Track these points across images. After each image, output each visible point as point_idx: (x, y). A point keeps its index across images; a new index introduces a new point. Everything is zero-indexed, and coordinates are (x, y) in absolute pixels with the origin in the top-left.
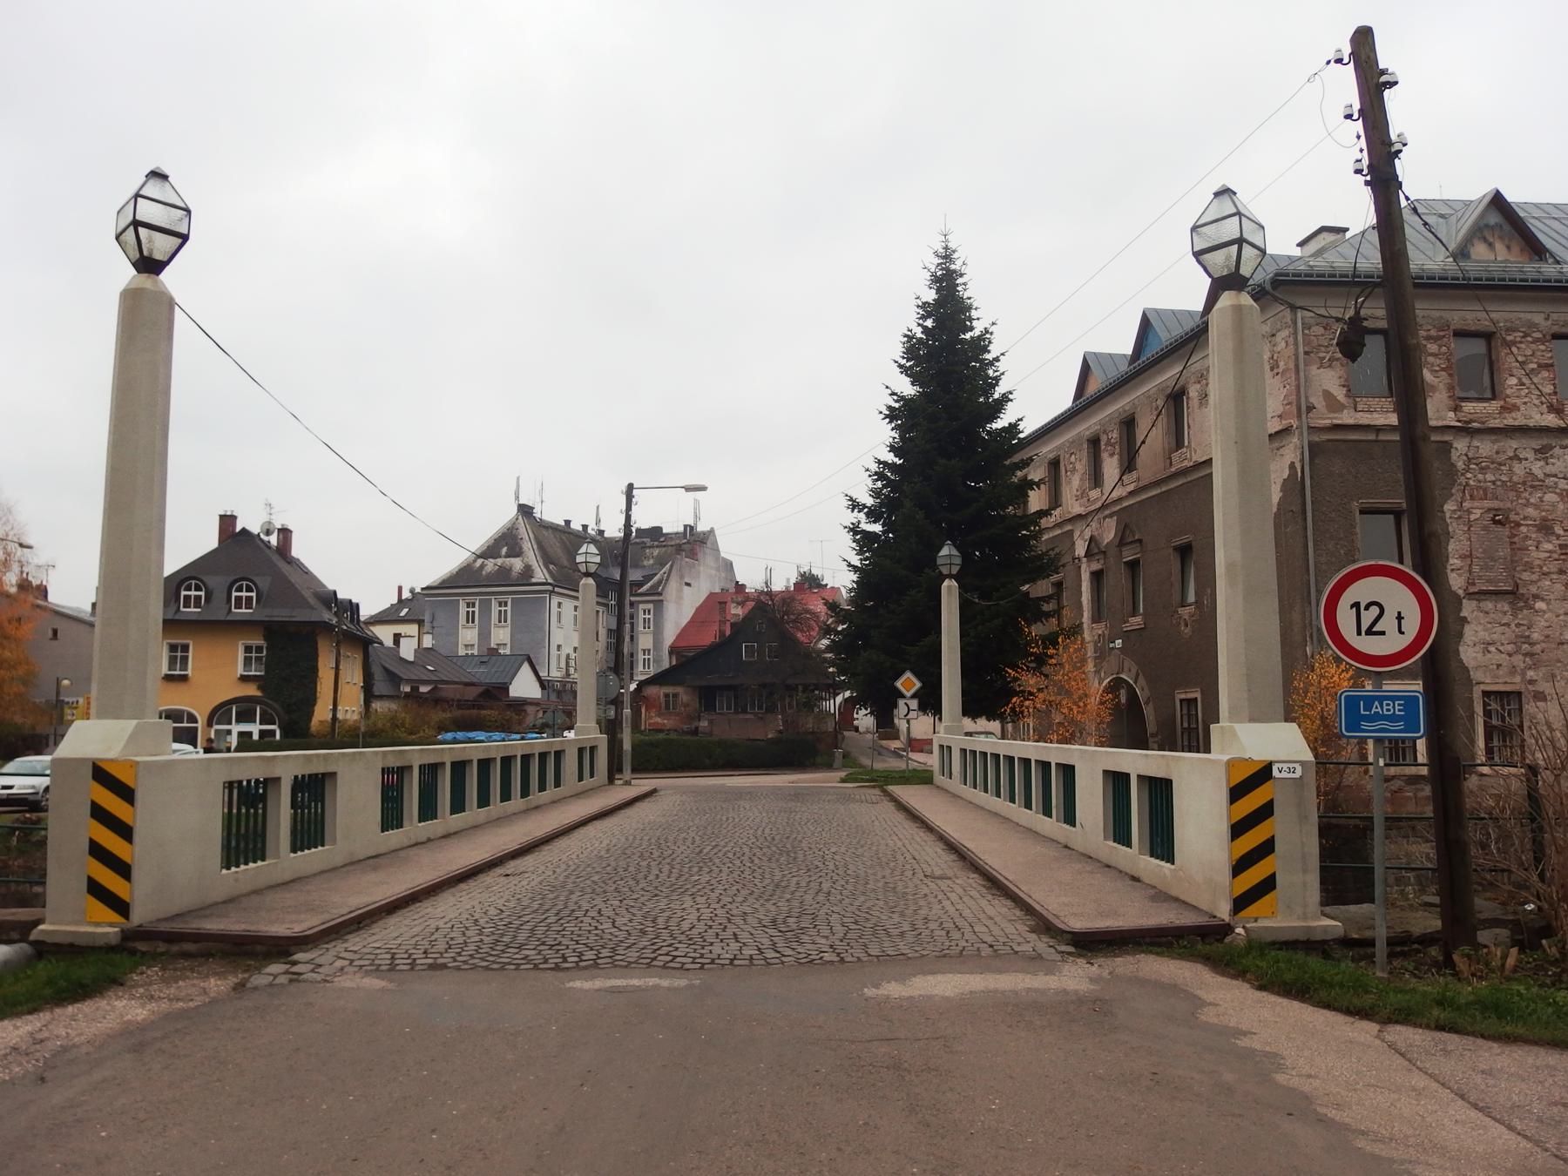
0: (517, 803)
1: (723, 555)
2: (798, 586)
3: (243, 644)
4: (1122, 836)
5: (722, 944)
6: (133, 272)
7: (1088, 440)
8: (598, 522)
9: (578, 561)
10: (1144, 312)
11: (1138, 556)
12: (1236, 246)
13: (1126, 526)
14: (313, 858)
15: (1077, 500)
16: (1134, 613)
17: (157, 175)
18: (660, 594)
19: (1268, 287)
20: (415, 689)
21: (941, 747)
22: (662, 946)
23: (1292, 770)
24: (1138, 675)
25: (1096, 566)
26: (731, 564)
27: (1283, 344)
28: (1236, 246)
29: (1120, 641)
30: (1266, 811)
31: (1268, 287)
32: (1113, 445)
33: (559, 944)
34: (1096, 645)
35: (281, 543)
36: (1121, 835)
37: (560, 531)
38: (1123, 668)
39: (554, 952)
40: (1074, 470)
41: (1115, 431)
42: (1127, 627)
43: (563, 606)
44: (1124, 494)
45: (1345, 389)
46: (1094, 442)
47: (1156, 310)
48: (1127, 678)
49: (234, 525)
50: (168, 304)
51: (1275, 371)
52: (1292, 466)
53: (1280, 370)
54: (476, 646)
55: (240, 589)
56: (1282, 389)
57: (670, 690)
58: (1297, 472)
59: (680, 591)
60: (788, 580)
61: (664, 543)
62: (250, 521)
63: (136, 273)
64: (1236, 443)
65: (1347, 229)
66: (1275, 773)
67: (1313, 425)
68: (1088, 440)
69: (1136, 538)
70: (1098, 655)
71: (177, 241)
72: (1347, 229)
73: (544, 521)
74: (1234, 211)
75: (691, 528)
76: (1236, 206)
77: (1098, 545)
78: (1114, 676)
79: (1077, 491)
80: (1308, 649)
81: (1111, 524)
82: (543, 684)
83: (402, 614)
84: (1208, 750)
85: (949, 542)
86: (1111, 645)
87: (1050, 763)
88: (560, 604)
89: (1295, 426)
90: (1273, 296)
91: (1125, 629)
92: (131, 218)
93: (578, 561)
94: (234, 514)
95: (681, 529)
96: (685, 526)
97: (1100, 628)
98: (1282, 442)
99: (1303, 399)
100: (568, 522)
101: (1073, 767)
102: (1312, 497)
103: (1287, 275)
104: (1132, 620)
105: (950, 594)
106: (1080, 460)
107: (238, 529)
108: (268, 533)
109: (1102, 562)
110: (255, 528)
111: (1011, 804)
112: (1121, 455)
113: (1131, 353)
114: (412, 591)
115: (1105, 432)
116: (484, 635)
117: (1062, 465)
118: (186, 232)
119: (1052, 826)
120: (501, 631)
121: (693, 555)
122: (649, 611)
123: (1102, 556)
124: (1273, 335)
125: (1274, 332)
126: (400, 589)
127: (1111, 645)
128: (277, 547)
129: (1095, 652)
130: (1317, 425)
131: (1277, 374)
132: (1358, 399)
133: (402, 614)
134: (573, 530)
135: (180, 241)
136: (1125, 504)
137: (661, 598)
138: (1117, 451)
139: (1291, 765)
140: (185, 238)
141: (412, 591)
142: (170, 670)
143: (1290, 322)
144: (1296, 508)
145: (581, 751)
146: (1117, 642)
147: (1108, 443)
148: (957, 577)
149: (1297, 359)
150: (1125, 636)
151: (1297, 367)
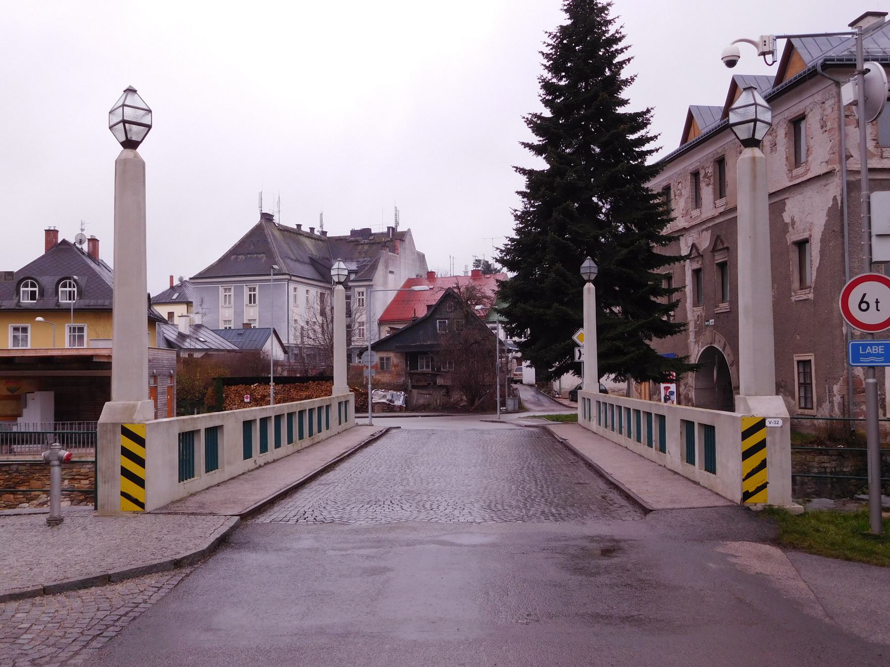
0: (307, 441)
1: (417, 250)
2: (475, 274)
3: (68, 326)
4: (690, 459)
5: (464, 517)
6: (122, 148)
7: (691, 173)
8: (321, 226)
9: (332, 274)
10: (733, 77)
11: (726, 259)
12: (753, 123)
13: (718, 237)
14: (217, 476)
15: (682, 217)
16: (723, 300)
17: (131, 91)
18: (371, 280)
19: (819, 69)
20: (191, 355)
21: (584, 399)
22: (432, 518)
23: (777, 422)
24: (725, 345)
25: (696, 266)
26: (424, 256)
27: (830, 110)
28: (753, 123)
29: (713, 320)
30: (762, 445)
31: (819, 69)
32: (709, 178)
33: (376, 518)
34: (695, 323)
35: (91, 250)
36: (690, 459)
37: (293, 233)
38: (715, 340)
39: (375, 522)
40: (681, 195)
41: (710, 167)
42: (717, 310)
43: (298, 290)
44: (717, 214)
45: (875, 142)
46: (696, 175)
47: (742, 76)
48: (718, 348)
49: (56, 238)
50: (141, 165)
51: (825, 129)
52: (835, 198)
53: (828, 128)
54: (233, 321)
55: (65, 286)
56: (828, 142)
57: (384, 355)
58: (838, 203)
59: (386, 277)
60: (466, 266)
61: (373, 241)
62: (67, 234)
63: (123, 149)
64: (750, 237)
65: (886, 14)
66: (767, 424)
67: (850, 169)
68: (691, 173)
69: (725, 246)
70: (697, 330)
71: (145, 129)
72: (886, 14)
73: (282, 226)
74: (753, 102)
75: (393, 229)
76: (755, 99)
77: (697, 250)
78: (709, 345)
79: (683, 210)
80: (843, 329)
81: (707, 236)
82: (285, 350)
83: (175, 297)
84: (733, 410)
85: (589, 257)
86: (707, 323)
87: (651, 413)
88: (295, 289)
89: (837, 170)
90: (823, 75)
91: (716, 312)
92: (122, 119)
93: (332, 274)
94: (56, 229)
95: (386, 230)
96: (389, 228)
97: (699, 310)
98: (828, 181)
99: (843, 149)
100: (299, 226)
101: (664, 417)
102: (848, 220)
103: (833, 60)
104: (721, 305)
105: (589, 292)
106: (685, 188)
107: (59, 240)
108: (81, 242)
109: (700, 262)
110: (72, 240)
111: (629, 439)
112: (714, 184)
113: (724, 106)
114: (181, 280)
115: (703, 168)
116: (239, 313)
117: (672, 192)
118: (150, 124)
119: (653, 453)
120: (252, 310)
121: (394, 250)
122: (363, 293)
123: (701, 258)
124: (823, 103)
125: (824, 100)
126: (172, 278)
127: (707, 323)
128: (88, 253)
129: (695, 328)
130: (854, 169)
131: (826, 131)
132: (884, 149)
133: (175, 297)
134: (303, 232)
135: (147, 129)
136: (717, 221)
137: (371, 283)
138: (712, 182)
139: (776, 420)
140: (149, 127)
141: (181, 280)
142: (14, 346)
143: (835, 94)
144: (837, 228)
145: (340, 404)
146: (711, 321)
147: (706, 176)
148: (594, 282)
149: (840, 119)
150: (717, 316)
151: (840, 126)
